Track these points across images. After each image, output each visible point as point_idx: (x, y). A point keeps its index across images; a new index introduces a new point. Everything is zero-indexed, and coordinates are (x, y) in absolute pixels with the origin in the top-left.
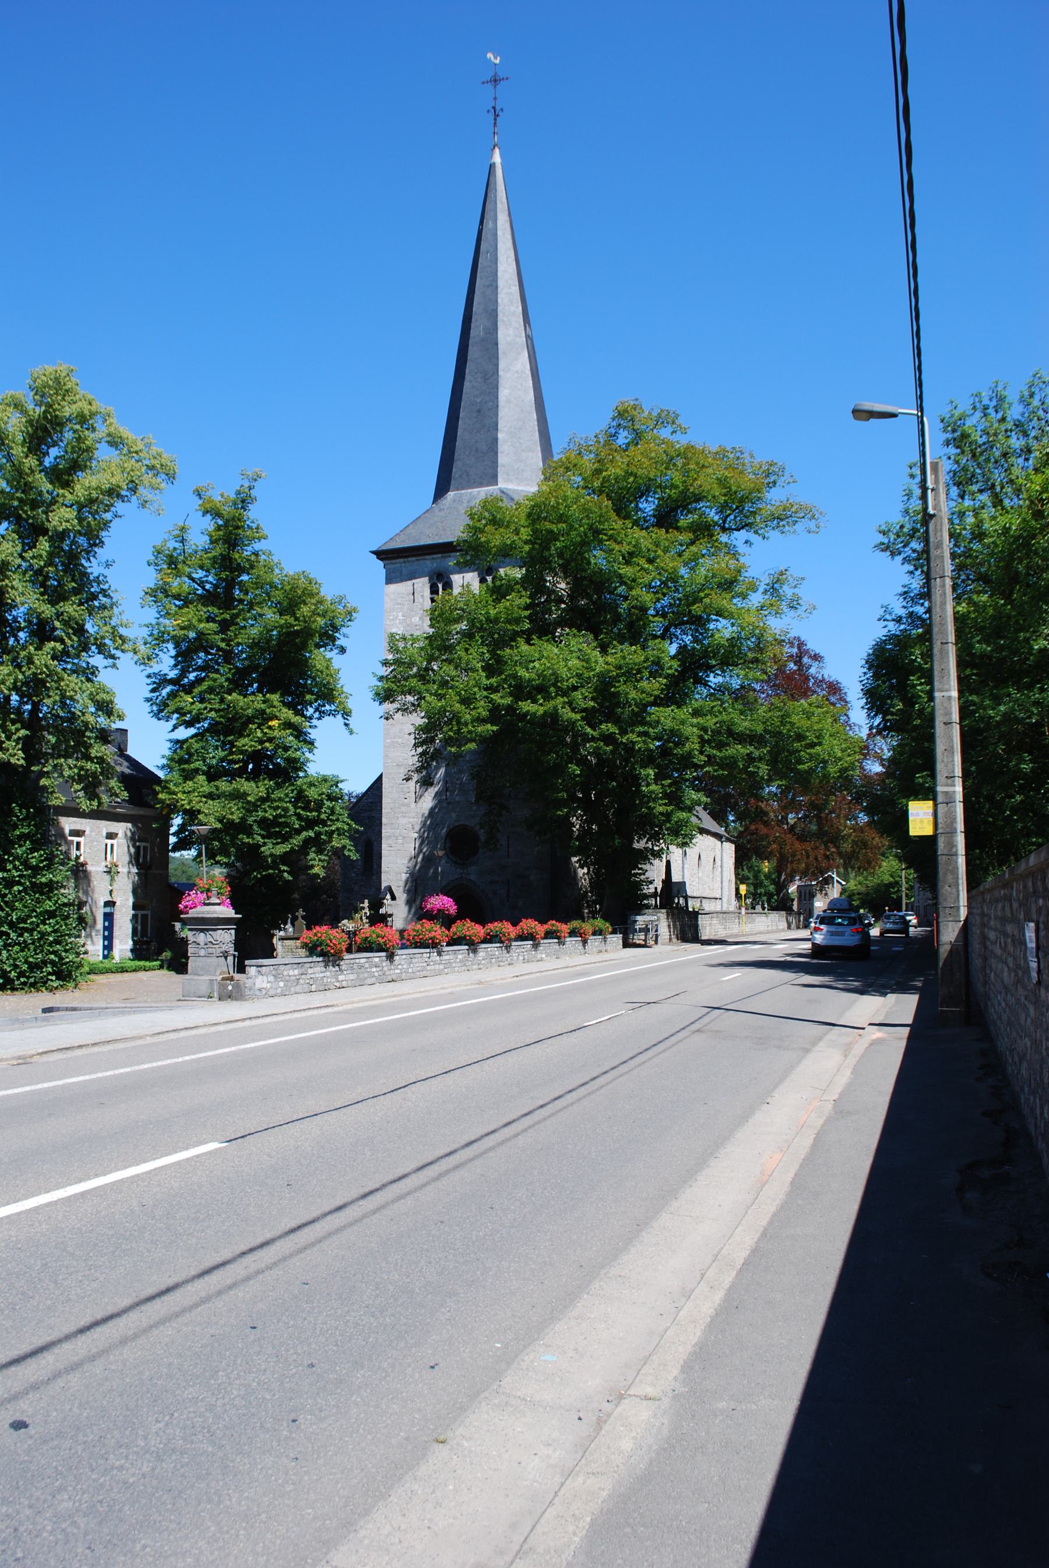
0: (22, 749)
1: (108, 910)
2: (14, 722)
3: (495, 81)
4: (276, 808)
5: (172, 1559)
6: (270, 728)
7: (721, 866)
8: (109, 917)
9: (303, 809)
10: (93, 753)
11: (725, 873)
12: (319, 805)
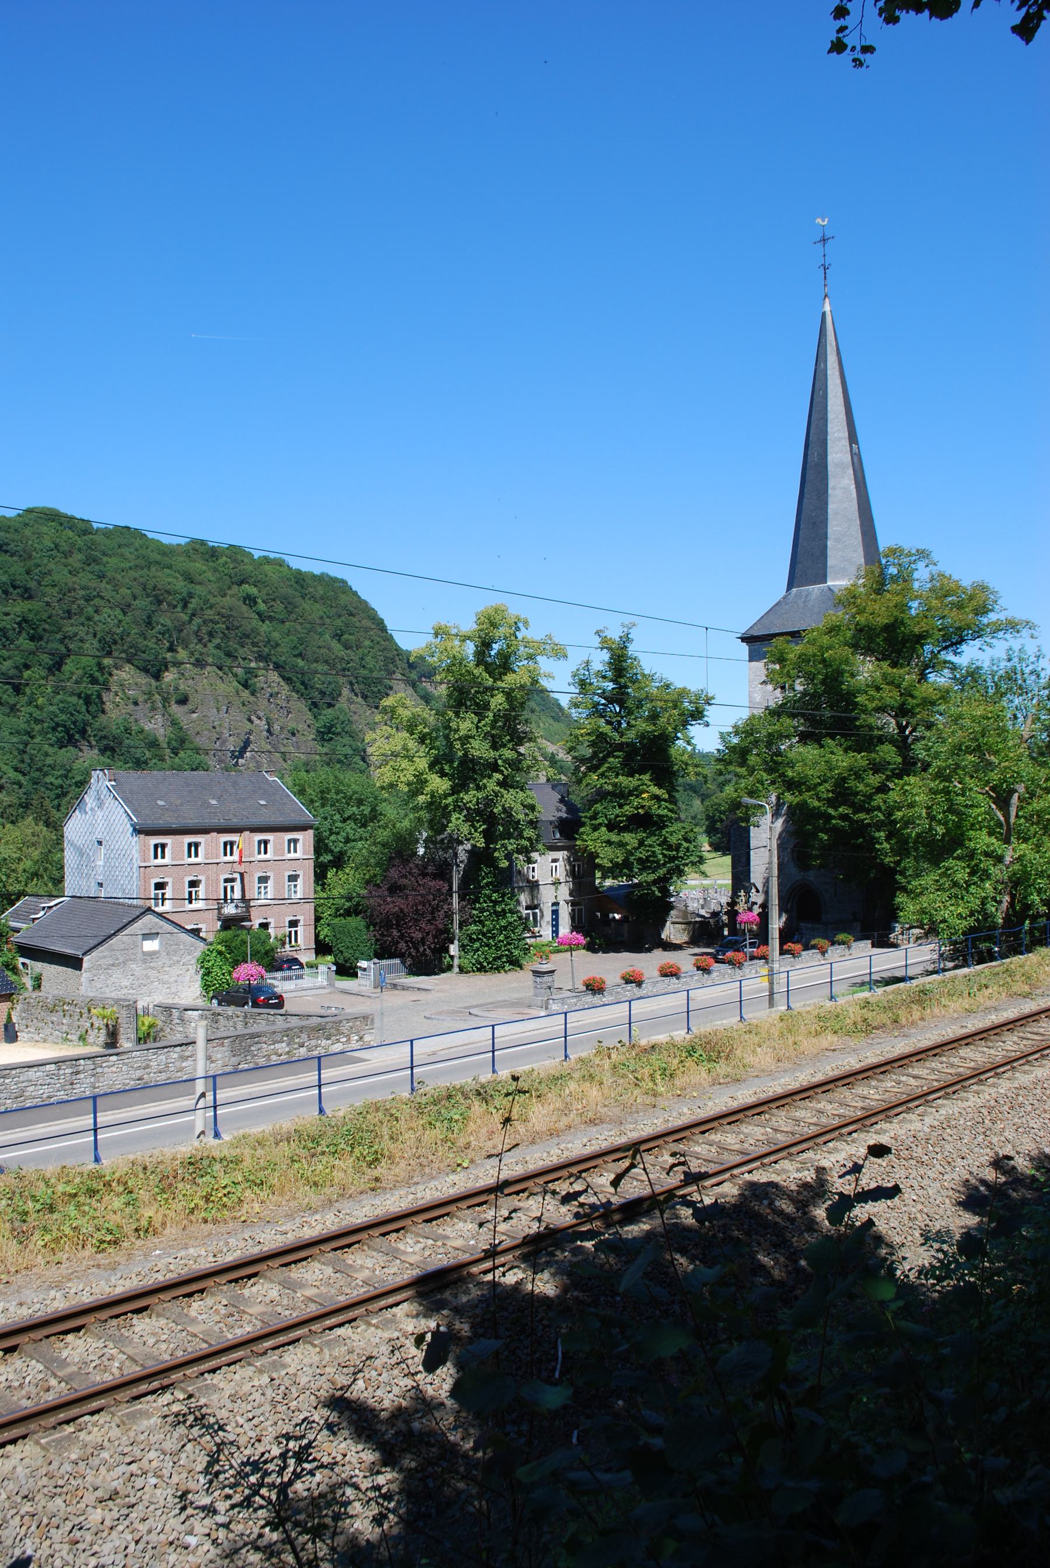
0: (484, 837)
1: (554, 908)
2: (478, 821)
3: (824, 240)
4: (648, 851)
6: (643, 799)
8: (555, 913)
9: (667, 850)
10: (525, 834)
12: (678, 847)
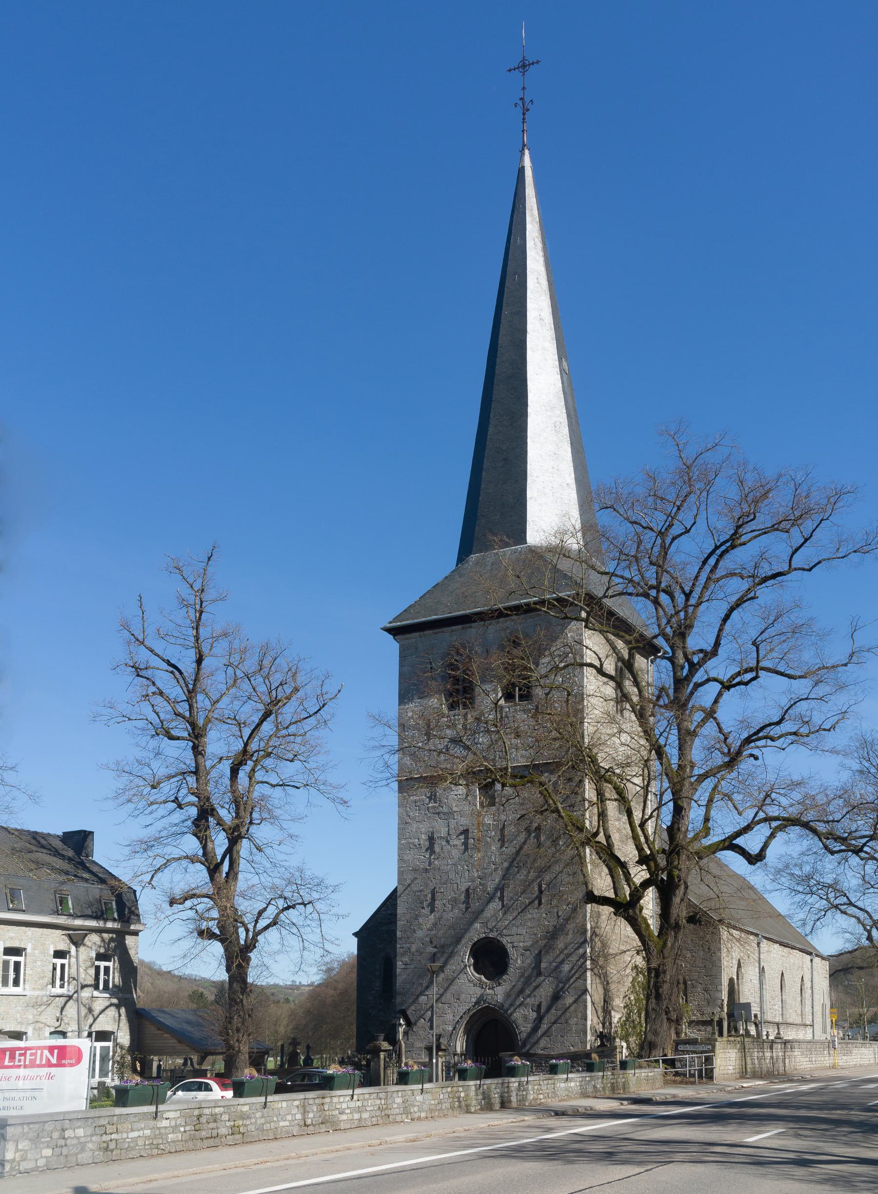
3: (524, 66)
5: (282, 804)
7: (812, 988)
11: (816, 996)
